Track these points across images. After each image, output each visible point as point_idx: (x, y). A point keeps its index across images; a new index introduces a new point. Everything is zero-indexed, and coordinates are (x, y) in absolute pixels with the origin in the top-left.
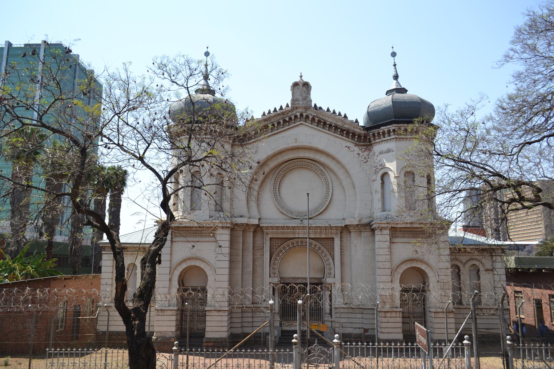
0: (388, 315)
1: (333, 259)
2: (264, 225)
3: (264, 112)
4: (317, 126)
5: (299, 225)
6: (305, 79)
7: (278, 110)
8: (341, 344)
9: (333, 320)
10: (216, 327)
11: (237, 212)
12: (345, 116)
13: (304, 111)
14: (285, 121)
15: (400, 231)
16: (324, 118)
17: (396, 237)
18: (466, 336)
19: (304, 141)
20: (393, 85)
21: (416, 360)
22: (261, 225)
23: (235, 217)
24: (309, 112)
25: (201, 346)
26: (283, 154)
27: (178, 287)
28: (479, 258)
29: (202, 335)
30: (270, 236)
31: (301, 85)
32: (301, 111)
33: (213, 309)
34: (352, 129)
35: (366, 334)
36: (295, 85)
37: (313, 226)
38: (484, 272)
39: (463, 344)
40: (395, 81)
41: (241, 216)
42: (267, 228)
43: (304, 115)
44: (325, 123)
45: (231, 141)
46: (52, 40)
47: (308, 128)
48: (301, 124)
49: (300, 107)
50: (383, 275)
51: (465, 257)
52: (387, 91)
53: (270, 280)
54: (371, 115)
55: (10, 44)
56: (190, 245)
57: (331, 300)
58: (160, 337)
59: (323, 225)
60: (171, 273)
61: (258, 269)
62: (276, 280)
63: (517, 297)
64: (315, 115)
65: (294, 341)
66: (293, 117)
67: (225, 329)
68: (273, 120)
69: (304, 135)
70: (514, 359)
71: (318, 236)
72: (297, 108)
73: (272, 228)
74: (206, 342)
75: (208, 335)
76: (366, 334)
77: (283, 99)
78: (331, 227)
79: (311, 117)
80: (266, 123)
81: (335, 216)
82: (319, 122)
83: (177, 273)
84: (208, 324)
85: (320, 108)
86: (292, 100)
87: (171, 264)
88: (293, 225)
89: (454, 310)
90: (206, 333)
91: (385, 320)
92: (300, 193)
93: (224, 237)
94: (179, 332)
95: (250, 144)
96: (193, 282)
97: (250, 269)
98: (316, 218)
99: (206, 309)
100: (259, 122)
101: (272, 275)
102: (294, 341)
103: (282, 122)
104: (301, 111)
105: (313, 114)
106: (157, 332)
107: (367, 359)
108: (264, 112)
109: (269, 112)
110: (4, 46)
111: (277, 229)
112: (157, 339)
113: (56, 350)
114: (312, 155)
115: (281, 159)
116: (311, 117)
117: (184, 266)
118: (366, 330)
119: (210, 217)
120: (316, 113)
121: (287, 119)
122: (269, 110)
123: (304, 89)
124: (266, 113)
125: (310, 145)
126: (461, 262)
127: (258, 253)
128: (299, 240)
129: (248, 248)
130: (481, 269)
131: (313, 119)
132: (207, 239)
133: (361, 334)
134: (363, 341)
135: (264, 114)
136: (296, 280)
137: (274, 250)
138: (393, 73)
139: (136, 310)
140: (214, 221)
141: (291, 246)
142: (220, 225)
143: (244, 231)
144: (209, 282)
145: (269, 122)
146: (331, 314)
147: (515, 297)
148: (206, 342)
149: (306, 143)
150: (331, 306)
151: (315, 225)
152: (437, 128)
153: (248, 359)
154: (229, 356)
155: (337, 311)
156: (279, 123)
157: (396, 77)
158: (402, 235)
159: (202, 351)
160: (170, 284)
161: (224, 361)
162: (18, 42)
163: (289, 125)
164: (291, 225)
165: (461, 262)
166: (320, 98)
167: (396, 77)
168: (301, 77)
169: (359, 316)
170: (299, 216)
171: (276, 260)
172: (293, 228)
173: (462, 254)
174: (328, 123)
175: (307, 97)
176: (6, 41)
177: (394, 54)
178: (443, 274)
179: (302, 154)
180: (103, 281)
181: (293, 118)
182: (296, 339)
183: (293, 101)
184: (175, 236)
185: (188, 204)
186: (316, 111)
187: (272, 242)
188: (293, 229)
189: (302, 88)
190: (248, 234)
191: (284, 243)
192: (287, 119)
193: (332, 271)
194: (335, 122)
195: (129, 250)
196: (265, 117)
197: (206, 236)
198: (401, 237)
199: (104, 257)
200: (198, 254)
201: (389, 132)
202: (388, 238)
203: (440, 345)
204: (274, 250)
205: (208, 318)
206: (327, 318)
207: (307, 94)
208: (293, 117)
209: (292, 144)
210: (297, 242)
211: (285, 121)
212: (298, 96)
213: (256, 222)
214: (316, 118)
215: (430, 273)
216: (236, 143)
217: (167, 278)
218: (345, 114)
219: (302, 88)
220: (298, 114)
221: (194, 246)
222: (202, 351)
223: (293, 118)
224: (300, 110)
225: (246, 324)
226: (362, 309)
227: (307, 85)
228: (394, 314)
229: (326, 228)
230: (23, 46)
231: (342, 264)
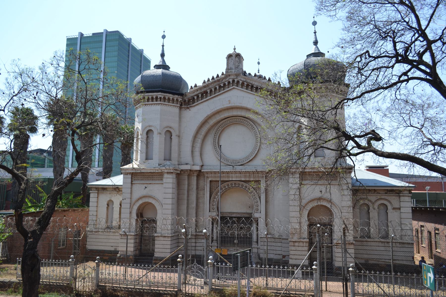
0: (297, 244)
1: (260, 198)
2: (205, 171)
3: (204, 81)
4: (247, 89)
5: (232, 170)
6: (238, 51)
7: (215, 78)
8: (214, 264)
9: (259, 247)
10: (162, 248)
11: (183, 160)
12: (269, 80)
13: (235, 77)
14: (220, 87)
15: (309, 175)
16: (251, 82)
17: (305, 180)
18: (180, 256)
19: (236, 102)
20: (312, 49)
21: (400, 288)
22: (202, 171)
23: (182, 165)
24: (239, 78)
25: (151, 263)
26: (220, 114)
27: (136, 218)
28: (386, 197)
29: (152, 254)
30: (210, 179)
31: (234, 56)
32: (235, 77)
33: (160, 235)
34: (275, 90)
35: (284, 259)
36: (230, 56)
37: (243, 171)
38: (392, 210)
39: (312, 269)
40: (314, 47)
41: (187, 164)
42: (207, 173)
43: (236, 80)
44: (252, 87)
45: (179, 105)
46: (110, 29)
47: (239, 91)
48: (234, 88)
49: (232, 75)
50: (294, 213)
51: (374, 197)
52: (307, 56)
53: (210, 214)
54: (292, 76)
55: (82, 35)
56: (144, 186)
57: (257, 231)
58: (122, 255)
59: (251, 171)
60: (131, 207)
61: (201, 205)
62: (214, 214)
63: (437, 233)
64: (244, 80)
65: (179, 260)
66: (227, 83)
67: (169, 251)
68: (210, 87)
69: (236, 97)
70: (356, 283)
71: (247, 179)
72: (229, 75)
73: (211, 173)
74: (155, 260)
75: (156, 255)
76: (284, 259)
77: (219, 68)
78: (258, 172)
79: (241, 82)
80: (205, 89)
81: (259, 164)
82: (248, 85)
83: (135, 208)
84: (156, 246)
85: (250, 74)
86: (226, 69)
87: (131, 201)
88: (227, 171)
89: (354, 242)
90: (155, 253)
91: (293, 248)
92: (236, 144)
93: (169, 181)
94: (137, 252)
95: (194, 106)
96: (148, 215)
97: (194, 205)
98: (246, 164)
99: (156, 235)
100: (201, 88)
101: (211, 210)
102: (179, 260)
103: (218, 87)
104: (235, 77)
105: (242, 79)
106: (121, 251)
107: (279, 279)
108: (204, 81)
109: (209, 80)
110: (78, 36)
111: (215, 174)
112: (120, 256)
113: (59, 261)
114: (243, 113)
115: (226, 114)
116: (241, 82)
117: (140, 202)
118: (284, 257)
119: (159, 165)
120: (245, 78)
121: (222, 85)
122: (209, 79)
123: (237, 59)
124: (206, 80)
125: (241, 105)
126: (370, 201)
127: (201, 193)
128: (233, 183)
129: (193, 188)
130: (389, 207)
131: (243, 84)
132: (157, 182)
133: (280, 259)
134: (280, 266)
135: (204, 82)
136: (231, 215)
137: (214, 190)
138: (313, 39)
139: (34, 232)
140: (161, 168)
141: (227, 187)
142: (166, 171)
143: (189, 176)
144: (158, 214)
145: (207, 88)
146: (257, 242)
147: (436, 233)
148: (155, 260)
149: (238, 104)
150: (257, 235)
151: (244, 170)
152: (348, 86)
153: (161, 273)
154: (156, 270)
155: (262, 240)
156: (215, 89)
157: (316, 43)
158: (310, 178)
159: (145, 266)
160: (130, 216)
161: (152, 274)
162: (88, 33)
163: (224, 90)
164: (225, 171)
165: (370, 201)
166: (249, 67)
167: (316, 43)
168: (235, 49)
169: (279, 244)
170: (234, 163)
171: (214, 198)
172: (228, 173)
173: (372, 194)
174: (255, 86)
175: (239, 66)
176: (104, 30)
177: (164, 37)
178: (345, 211)
179: (235, 113)
180: (90, 213)
181: (227, 84)
182: (316, 266)
183: (228, 69)
184: (134, 180)
185: (144, 155)
186: (245, 77)
187: (212, 184)
188: (227, 174)
189: (235, 58)
190: (193, 177)
191: (221, 185)
192: (222, 85)
193: (259, 208)
194: (260, 85)
195: (108, 190)
196: (205, 84)
197: (156, 180)
198: (310, 180)
199: (91, 195)
200: (150, 194)
201: (157, 98)
202: (297, 180)
203: (293, 268)
204: (214, 190)
205: (156, 242)
206: (254, 245)
207: (239, 63)
208: (227, 83)
209: (227, 105)
210: (232, 184)
211: (220, 87)
212: (231, 65)
213: (197, 168)
214: (245, 83)
215: (335, 210)
216: (183, 106)
217: (128, 211)
218: (269, 78)
219: (235, 58)
220: (231, 81)
221: (146, 187)
222: (145, 266)
223: (227, 84)
224: (232, 77)
225: (199, 248)
226: (281, 239)
227: (238, 56)
228: (301, 244)
229: (253, 172)
230: (91, 35)
231: (266, 202)
